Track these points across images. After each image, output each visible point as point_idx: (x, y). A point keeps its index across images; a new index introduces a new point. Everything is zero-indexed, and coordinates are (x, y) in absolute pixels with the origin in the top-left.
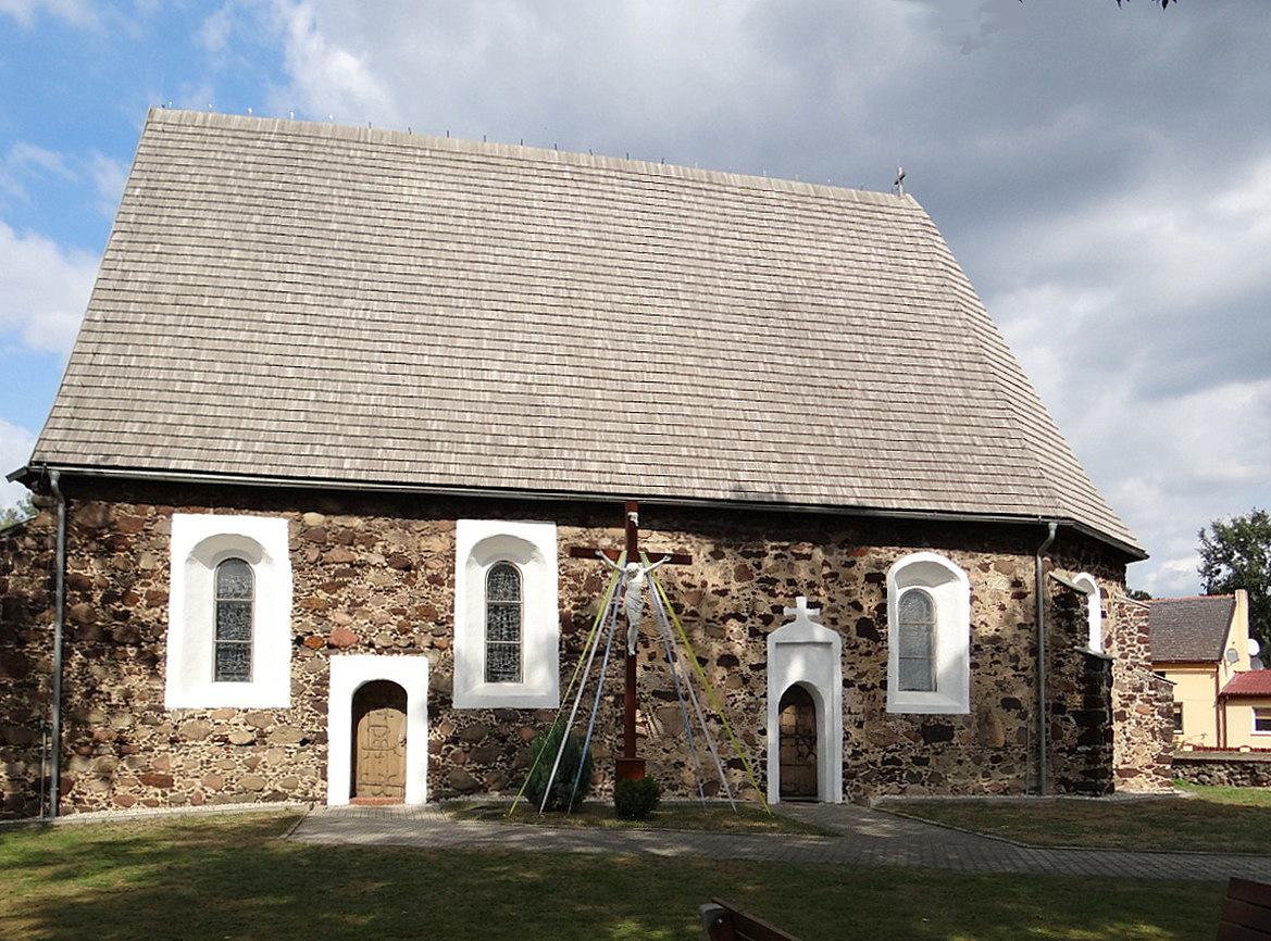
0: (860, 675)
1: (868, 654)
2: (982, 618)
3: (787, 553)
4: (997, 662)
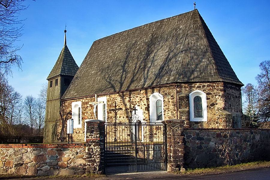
2: (166, 104)
3: (135, 97)
4: (169, 113)
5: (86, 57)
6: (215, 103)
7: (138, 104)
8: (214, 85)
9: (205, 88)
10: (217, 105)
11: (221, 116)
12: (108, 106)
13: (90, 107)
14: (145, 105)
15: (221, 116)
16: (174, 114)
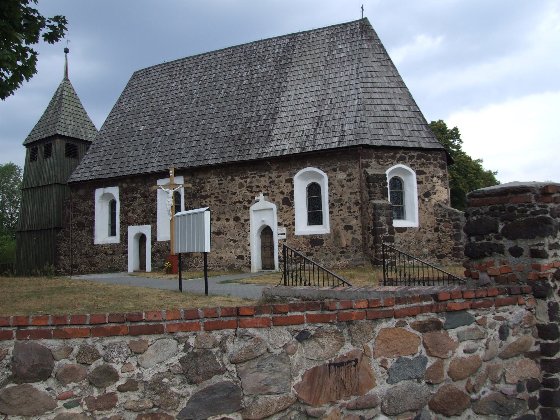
0: (284, 220)
1: (287, 211)
2: (334, 191)
4: (342, 210)
5: (120, 100)
6: (432, 192)
7: (266, 192)
8: (429, 155)
9: (413, 161)
10: (436, 196)
11: (447, 216)
12: (188, 196)
13: (142, 198)
14: (282, 193)
15: (447, 216)
16: (354, 212)
